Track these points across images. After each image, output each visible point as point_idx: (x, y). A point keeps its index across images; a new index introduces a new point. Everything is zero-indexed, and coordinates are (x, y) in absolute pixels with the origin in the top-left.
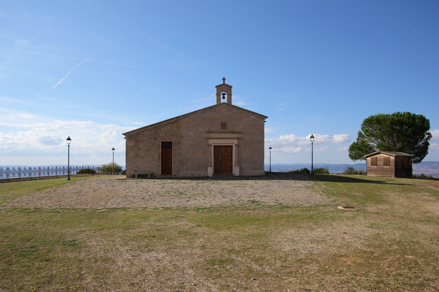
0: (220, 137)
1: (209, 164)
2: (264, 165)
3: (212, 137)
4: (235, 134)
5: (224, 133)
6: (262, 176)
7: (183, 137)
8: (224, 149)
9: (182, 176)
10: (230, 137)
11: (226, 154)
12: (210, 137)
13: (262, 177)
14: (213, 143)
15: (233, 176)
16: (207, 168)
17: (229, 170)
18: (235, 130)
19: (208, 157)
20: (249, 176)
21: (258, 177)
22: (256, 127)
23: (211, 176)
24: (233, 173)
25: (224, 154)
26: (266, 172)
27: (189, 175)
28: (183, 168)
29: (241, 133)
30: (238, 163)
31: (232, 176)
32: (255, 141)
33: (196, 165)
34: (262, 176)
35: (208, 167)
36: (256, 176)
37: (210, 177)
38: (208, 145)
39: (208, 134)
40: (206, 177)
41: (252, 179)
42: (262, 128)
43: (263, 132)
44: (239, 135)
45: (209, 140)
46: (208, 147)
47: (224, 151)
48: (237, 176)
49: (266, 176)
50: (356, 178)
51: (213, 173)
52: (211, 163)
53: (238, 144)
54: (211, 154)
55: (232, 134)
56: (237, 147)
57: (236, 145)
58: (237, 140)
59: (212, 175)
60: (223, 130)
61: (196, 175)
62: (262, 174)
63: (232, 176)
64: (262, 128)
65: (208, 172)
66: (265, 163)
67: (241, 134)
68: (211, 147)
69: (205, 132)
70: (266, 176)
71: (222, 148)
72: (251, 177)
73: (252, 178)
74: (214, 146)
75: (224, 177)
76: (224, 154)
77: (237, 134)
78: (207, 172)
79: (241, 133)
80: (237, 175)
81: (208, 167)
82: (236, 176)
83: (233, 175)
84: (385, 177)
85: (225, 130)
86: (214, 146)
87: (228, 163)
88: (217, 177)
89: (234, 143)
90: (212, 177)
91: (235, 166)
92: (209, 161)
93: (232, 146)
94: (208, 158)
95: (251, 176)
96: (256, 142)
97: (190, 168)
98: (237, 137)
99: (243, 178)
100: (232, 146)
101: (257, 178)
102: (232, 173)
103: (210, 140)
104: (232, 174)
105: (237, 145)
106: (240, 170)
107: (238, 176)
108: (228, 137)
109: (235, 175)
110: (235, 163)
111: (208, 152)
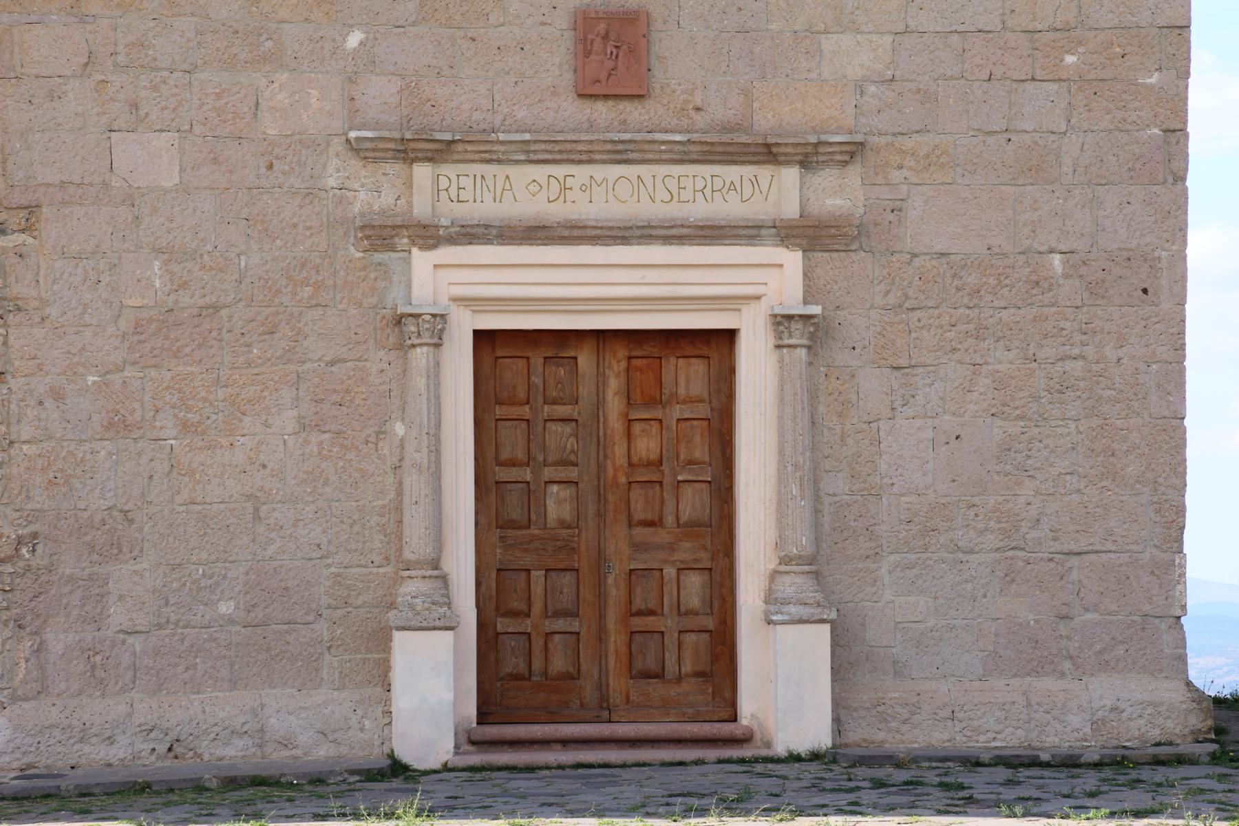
0: (557, 212)
1: (413, 588)
2: (1193, 598)
3: (445, 222)
4: (764, 173)
5: (621, 154)
6: (1158, 762)
7: (32, 209)
8: (614, 384)
9: (25, 774)
10: (699, 210)
11: (646, 446)
12: (421, 208)
13: (1160, 774)
14: (455, 299)
15: (746, 752)
16: (381, 640)
17: (687, 667)
18: (595, 391)
19: (400, 493)
20: (972, 763)
21: (1097, 765)
22: (1070, 59)
23: (434, 763)
24: (749, 705)
25: (619, 451)
26: (1218, 702)
27: (118, 752)
28: (39, 650)
29: (854, 151)
30: (817, 575)
31: (735, 753)
32: (1057, 259)
33: (225, 608)
34: (1158, 762)
35: (397, 635)
36: (1070, 763)
37: (421, 767)
38: (399, 320)
39: (394, 169)
40: (372, 775)
41: (1010, 794)
42: (1154, 79)
43: (1176, 133)
44: (826, 178)
45: (408, 263)
46: (403, 347)
47: (614, 405)
48: (794, 758)
49: (1215, 759)
50: (772, 438)
51: (471, 710)
52: (444, 579)
53: (815, 310)
54: (436, 450)
55: (732, 172)
56: (802, 353)
57: (782, 321)
58: (792, 260)
59: (450, 745)
60: (602, 111)
61: (229, 752)
62: (1155, 734)
63: (735, 753)
64: (1154, 79)
65: (403, 700)
66: (1194, 570)
67: (854, 174)
68: (437, 346)
69: (356, 149)
70: (1215, 759)
71: (585, 360)
72: (1003, 773)
73: (1010, 783)
74: (481, 337)
75: (624, 766)
76: (619, 451)
77: (791, 174)
78: (388, 702)
79: (854, 151)
80: (802, 746)
81: (397, 635)
82: (780, 750)
83: (745, 739)
84: (765, 431)
85: (634, 112)
86: (481, 337)
87: (670, 572)
88: (531, 769)
89: (758, 298)
90: (446, 768)
91: (770, 622)
92: (416, 543)
93: (729, 336)
94: (399, 509)
95: (1001, 761)
96: (1067, 276)
97: (136, 643)
98: (790, 210)
99: (879, 784)
100: (729, 336)
101: (1090, 780)
102: (734, 718)
103: (422, 261)
104: (726, 729)
105: (796, 326)
106: (840, 671)
107: (815, 756)
108: (675, 211)
109: (768, 745)
110: (774, 574)
111: (400, 429)
